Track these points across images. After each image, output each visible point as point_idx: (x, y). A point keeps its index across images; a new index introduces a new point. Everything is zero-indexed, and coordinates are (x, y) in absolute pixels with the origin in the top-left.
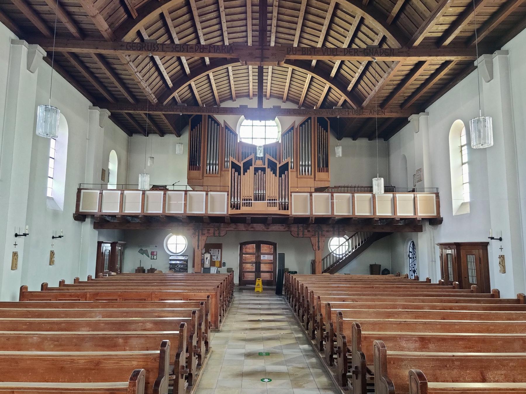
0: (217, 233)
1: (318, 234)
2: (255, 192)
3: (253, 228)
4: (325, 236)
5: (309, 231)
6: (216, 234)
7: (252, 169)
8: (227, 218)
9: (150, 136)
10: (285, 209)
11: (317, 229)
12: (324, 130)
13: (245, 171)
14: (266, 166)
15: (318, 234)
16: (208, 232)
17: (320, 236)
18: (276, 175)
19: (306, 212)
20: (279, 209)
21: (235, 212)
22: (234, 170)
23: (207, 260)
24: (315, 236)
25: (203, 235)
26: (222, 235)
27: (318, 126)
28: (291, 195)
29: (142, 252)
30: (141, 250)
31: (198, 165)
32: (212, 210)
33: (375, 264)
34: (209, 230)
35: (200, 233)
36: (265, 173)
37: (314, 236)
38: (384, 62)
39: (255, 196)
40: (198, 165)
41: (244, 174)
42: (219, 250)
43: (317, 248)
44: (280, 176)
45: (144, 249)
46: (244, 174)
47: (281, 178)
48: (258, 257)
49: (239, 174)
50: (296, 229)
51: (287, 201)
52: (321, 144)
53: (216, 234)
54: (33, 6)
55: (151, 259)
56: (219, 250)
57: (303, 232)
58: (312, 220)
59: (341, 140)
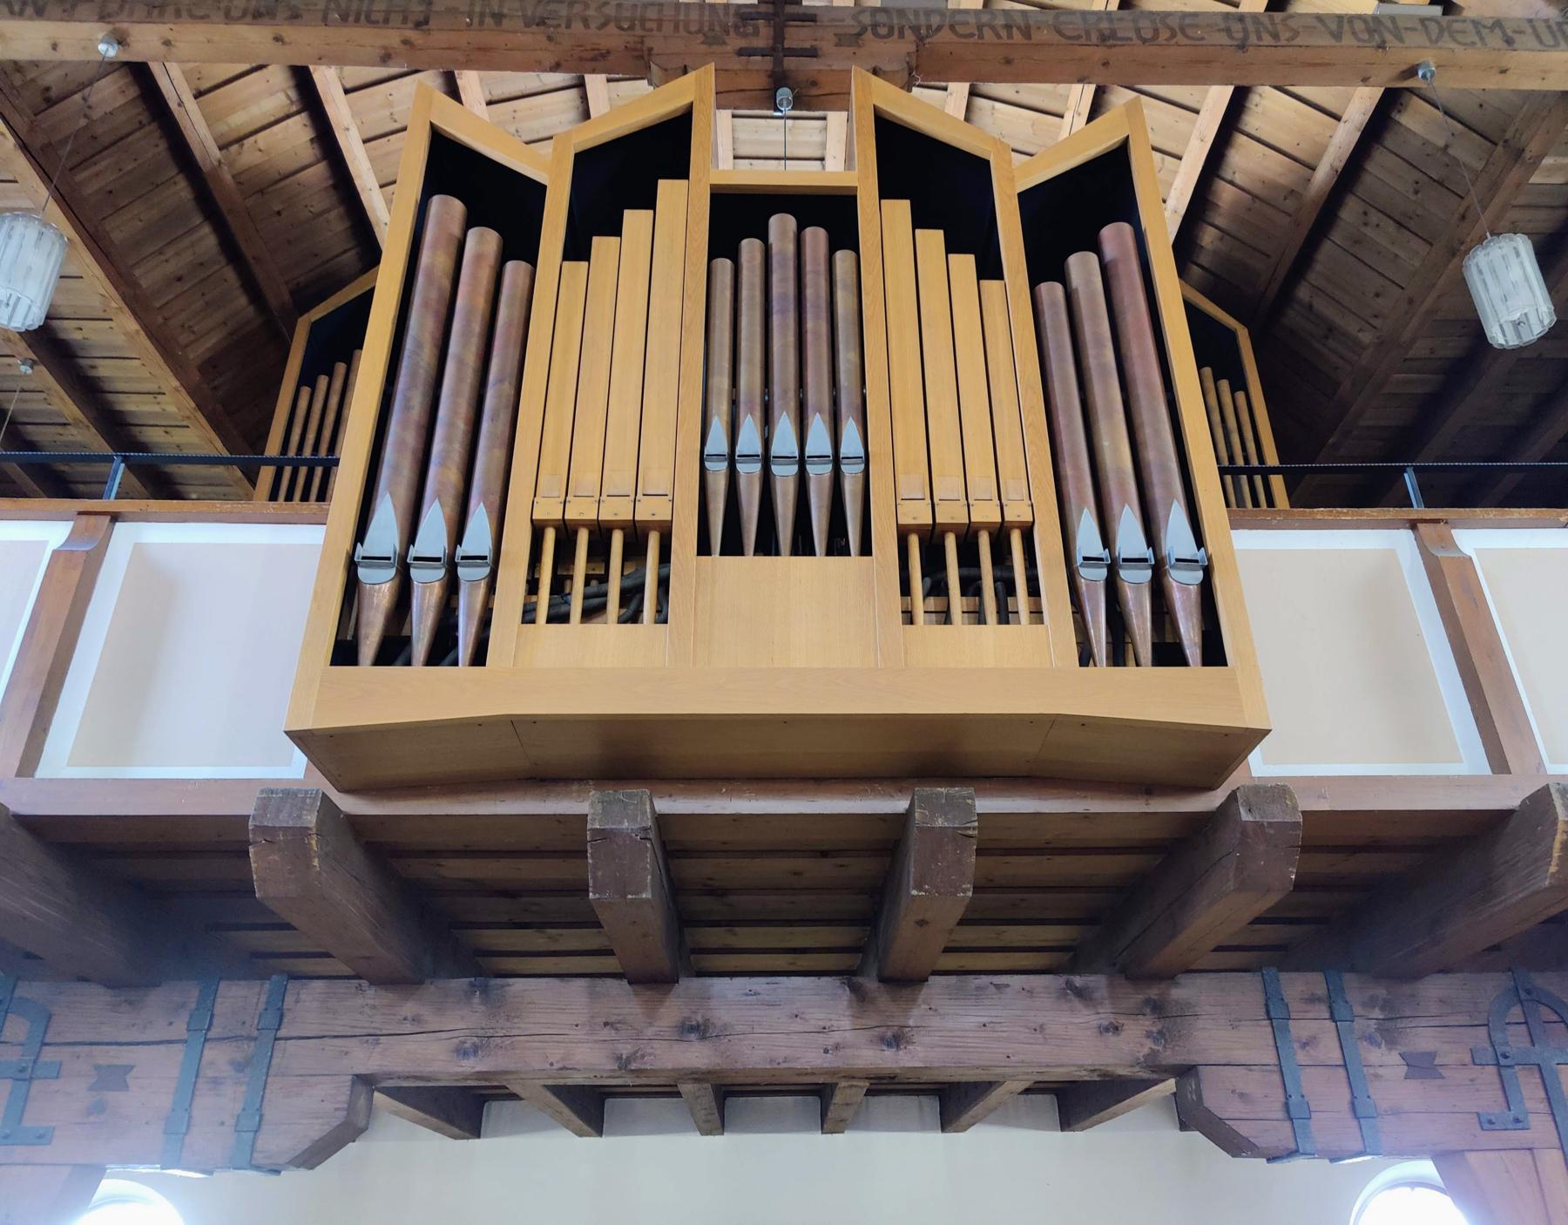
2: (718, 442)
3: (697, 1030)
8: (285, 820)
11: (1516, 1040)
14: (863, 179)
18: (990, 268)
39: (719, 485)
41: (577, 249)
46: (577, 249)
47: (1051, 291)
50: (1253, 1044)
54: (72, 486)
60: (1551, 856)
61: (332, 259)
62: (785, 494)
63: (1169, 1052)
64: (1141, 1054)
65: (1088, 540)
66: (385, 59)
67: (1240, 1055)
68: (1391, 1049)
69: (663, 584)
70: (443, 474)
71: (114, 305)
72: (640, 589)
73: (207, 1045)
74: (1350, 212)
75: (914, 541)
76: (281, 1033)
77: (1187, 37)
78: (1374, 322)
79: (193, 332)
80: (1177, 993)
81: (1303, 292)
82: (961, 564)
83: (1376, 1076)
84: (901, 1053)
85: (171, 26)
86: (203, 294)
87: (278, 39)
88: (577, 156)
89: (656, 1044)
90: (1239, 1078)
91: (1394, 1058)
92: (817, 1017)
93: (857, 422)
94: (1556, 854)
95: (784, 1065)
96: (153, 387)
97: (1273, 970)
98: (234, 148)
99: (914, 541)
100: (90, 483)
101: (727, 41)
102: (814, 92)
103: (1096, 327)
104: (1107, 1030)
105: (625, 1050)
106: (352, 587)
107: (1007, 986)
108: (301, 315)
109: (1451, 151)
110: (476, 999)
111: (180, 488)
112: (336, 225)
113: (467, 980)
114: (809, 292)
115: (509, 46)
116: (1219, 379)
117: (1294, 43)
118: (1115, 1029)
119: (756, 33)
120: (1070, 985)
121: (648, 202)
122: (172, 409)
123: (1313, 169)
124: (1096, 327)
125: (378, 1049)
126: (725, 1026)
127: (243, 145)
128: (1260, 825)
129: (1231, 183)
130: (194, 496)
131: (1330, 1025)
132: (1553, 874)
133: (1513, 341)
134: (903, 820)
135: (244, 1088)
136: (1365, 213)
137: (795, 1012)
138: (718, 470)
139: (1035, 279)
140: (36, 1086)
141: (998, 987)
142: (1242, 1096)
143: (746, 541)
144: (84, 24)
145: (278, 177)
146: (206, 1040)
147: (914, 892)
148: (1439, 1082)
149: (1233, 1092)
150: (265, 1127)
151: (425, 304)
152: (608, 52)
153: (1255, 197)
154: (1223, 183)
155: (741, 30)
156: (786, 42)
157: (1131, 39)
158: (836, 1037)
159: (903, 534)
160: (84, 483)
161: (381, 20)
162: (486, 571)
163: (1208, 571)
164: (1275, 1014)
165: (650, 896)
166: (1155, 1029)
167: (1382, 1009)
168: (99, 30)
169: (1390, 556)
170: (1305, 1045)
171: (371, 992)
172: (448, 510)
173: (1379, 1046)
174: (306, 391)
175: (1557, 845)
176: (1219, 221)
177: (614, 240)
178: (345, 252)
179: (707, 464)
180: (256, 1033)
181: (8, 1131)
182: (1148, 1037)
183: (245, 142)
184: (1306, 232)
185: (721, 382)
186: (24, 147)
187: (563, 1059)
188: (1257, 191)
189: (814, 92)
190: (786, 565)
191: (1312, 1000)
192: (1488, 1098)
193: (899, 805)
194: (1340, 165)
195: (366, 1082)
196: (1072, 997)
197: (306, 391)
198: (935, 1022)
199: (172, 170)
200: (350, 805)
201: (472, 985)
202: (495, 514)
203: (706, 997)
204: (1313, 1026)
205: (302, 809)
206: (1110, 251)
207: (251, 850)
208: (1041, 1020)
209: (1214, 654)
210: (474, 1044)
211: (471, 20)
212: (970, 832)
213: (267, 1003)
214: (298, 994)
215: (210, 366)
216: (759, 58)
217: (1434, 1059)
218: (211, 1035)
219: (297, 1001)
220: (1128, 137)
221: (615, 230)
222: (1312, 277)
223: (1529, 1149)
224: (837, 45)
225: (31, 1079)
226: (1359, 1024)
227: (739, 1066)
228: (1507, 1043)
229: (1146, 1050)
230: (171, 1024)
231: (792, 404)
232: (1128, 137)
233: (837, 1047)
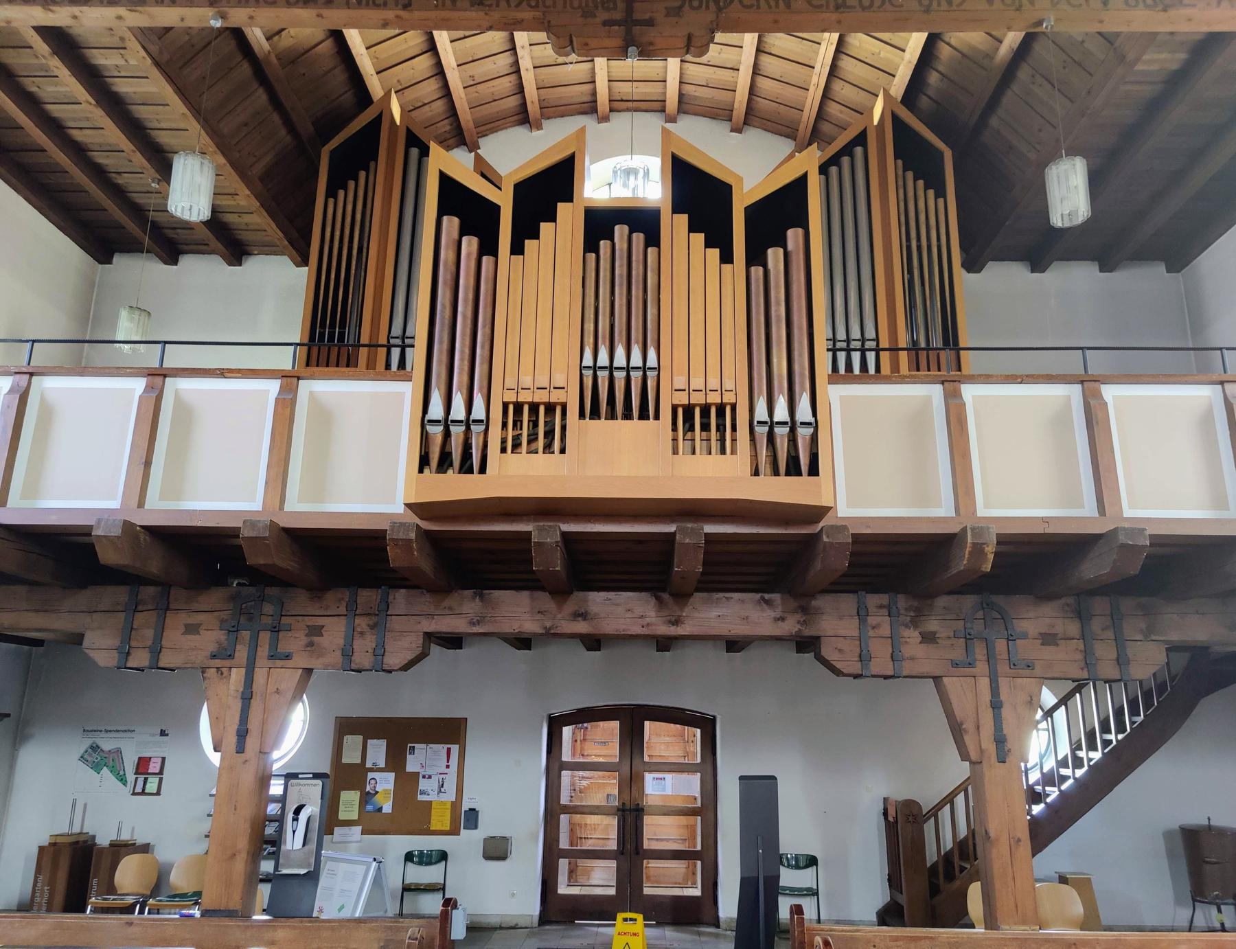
0: (363, 649)
1: (990, 657)
2: (588, 361)
3: (582, 615)
4: (1038, 670)
5: (929, 638)
6: (362, 656)
7: (569, 218)
8: (401, 536)
9: (186, 261)
10: (793, 469)
11: (978, 626)
12: (926, 188)
13: (525, 230)
15: (990, 657)
16: (311, 644)
17: (1003, 668)
18: (727, 258)
20: (756, 473)
22: (451, 224)
23: (295, 819)
24: (971, 665)
25: (279, 663)
26: (394, 659)
27: (900, 172)
29: (97, 759)
30: (95, 748)
33: (1210, 828)
34: (316, 631)
35: (263, 651)
36: (653, 239)
37: (963, 665)
38: (1099, 33)
39: (589, 382)
41: (517, 249)
42: (449, 750)
43: (989, 746)
44: (756, 256)
45: (107, 745)
46: (517, 249)
47: (757, 271)
48: (632, 782)
49: (489, 247)
50: (849, 627)
51: (804, 411)
52: (919, 248)
53: (362, 656)
55: (134, 794)
56: (449, 750)
57: (895, 641)
58: (978, 549)
59: (979, 271)
60: (964, 556)
61: (338, 98)
62: (620, 388)
63: (807, 630)
64: (794, 631)
65: (761, 413)
66: (385, 25)
67: (842, 632)
68: (915, 630)
69: (564, 428)
70: (459, 378)
71: (211, 150)
72: (553, 431)
73: (356, 617)
74: (1023, 74)
75: (680, 411)
76: (388, 613)
77: (893, 5)
78: (1037, 146)
79: (255, 156)
80: (814, 603)
81: (994, 121)
82: (701, 417)
83: (906, 642)
84: (679, 628)
85: (254, 9)
86: (260, 132)
87: (319, 16)
88: (514, 185)
89: (562, 622)
90: (841, 643)
91: (916, 634)
92: (638, 610)
93: (655, 348)
94: (967, 556)
95: (623, 633)
96: (232, 191)
97: (864, 593)
98: (276, 38)
99: (680, 411)
100: (190, 244)
101: (597, 14)
102: (651, 48)
103: (778, 294)
104: (778, 619)
105: (548, 624)
106: (425, 438)
107: (732, 598)
108: (324, 146)
109: (1086, 45)
110: (477, 599)
111: (248, 248)
112: (340, 76)
113: (472, 590)
114: (634, 273)
115: (461, 18)
116: (928, 189)
117: (961, 8)
118: (783, 619)
119: (615, 8)
120: (762, 598)
121: (552, 218)
122: (243, 203)
123: (1001, 42)
124: (778, 294)
125: (434, 621)
126: (596, 614)
127: (281, 36)
128: (831, 543)
129: (948, 44)
130: (256, 252)
131: (888, 618)
132: (965, 565)
133: (1067, 224)
134: (674, 534)
135: (375, 637)
136: (1033, 76)
137: (628, 608)
138: (588, 374)
139: (749, 263)
140: (281, 634)
141: (727, 598)
142: (840, 651)
143: (601, 411)
144: (202, 9)
145: (303, 51)
146: (355, 615)
147: (676, 569)
148: (936, 645)
149: (836, 648)
150: (386, 654)
151: (445, 283)
152: (522, 20)
153: (964, 55)
154: (943, 44)
155: (606, 5)
156: (634, 14)
157: (855, 7)
158: (648, 620)
159: (674, 409)
160: (187, 244)
161: (382, 3)
162: (484, 427)
163: (816, 428)
164: (862, 614)
165: (559, 569)
166: (802, 620)
167: (914, 611)
168: (210, 12)
169: (928, 399)
170: (873, 628)
171: (428, 595)
172: (465, 396)
173: (910, 629)
174: (331, 201)
175: (967, 552)
176: (940, 68)
177: (536, 241)
178: (346, 92)
179: (583, 372)
180: (377, 613)
181: (272, 654)
182: (798, 623)
183: (282, 33)
184: (643, 593)
185: (590, 326)
186: (157, 64)
187: (520, 628)
188: (965, 51)
189: (651, 48)
190: (620, 423)
191: (881, 607)
192: (958, 654)
193: (671, 528)
194: (1015, 46)
195: (430, 637)
196: (765, 605)
197: (331, 201)
198: (697, 615)
199: (255, 85)
200: (426, 525)
201: (475, 593)
202: (485, 399)
203: (586, 601)
204: (880, 622)
205: (408, 531)
206: (790, 246)
207: (388, 547)
208: (747, 614)
209: (814, 470)
210: (478, 620)
211: (437, 1)
212: (701, 545)
213: (381, 599)
214: (395, 595)
215: (265, 177)
216: (617, 27)
217: (935, 634)
218: (357, 613)
219: (394, 599)
220: (807, 172)
221: (536, 236)
222: (1000, 112)
223: (974, 677)
224: (666, 16)
225: (278, 631)
226: (902, 618)
227: (601, 633)
228: (972, 628)
229: (796, 629)
230: (338, 607)
231: (624, 339)
232: (807, 172)
233: (648, 624)
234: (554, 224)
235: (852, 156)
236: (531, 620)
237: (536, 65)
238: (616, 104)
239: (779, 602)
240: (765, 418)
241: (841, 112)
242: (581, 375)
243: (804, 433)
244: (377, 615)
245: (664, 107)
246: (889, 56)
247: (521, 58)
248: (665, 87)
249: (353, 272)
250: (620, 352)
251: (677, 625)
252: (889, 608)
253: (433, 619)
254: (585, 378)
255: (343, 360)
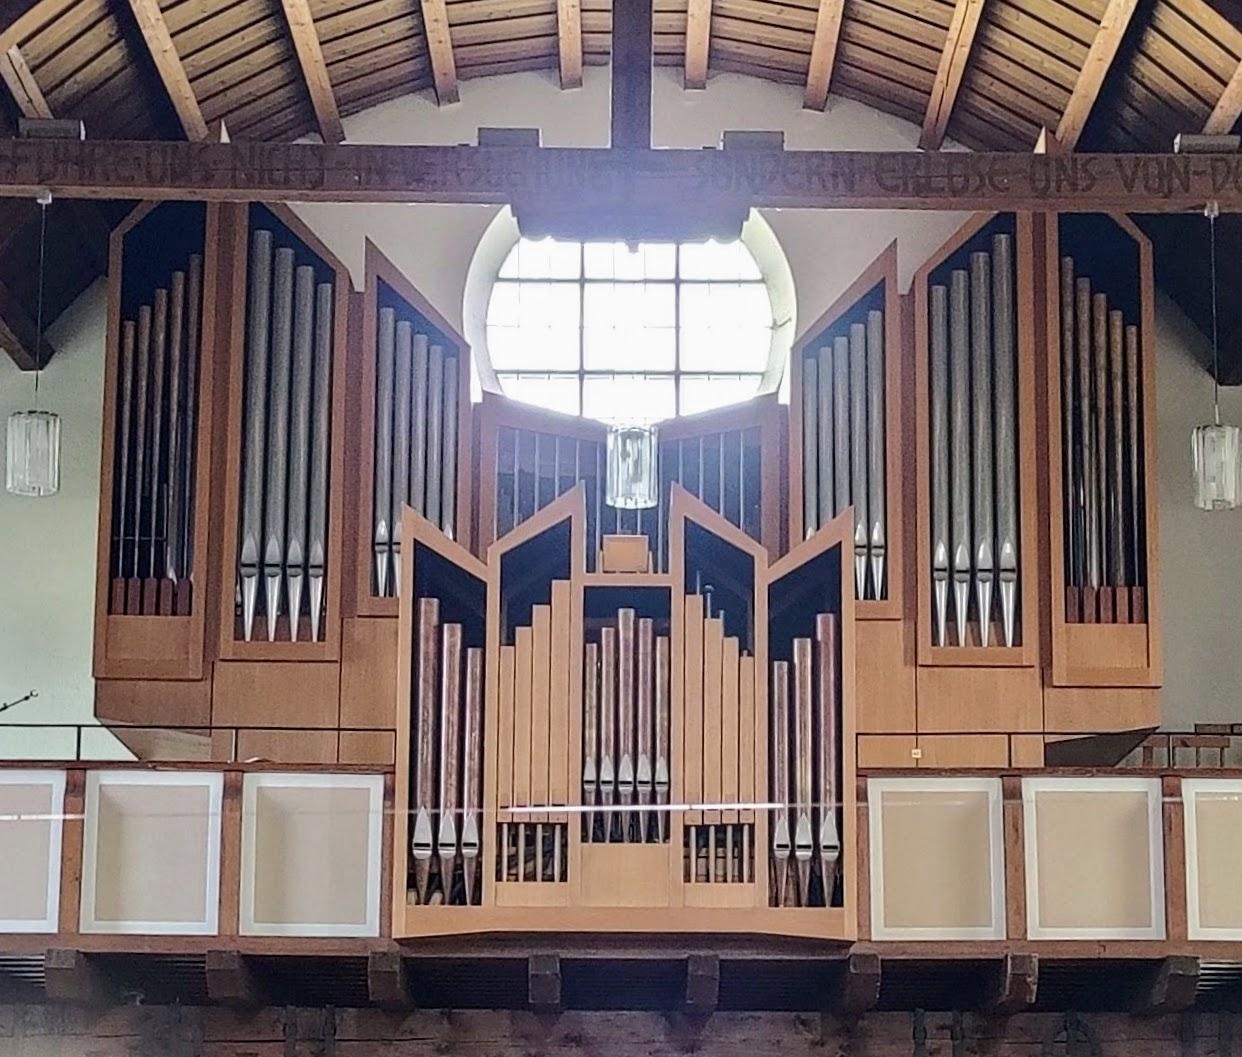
2: (590, 775)
7: (567, 595)
10: (815, 900)
12: (1110, 308)
13: (517, 616)
19: (972, 913)
20: (775, 902)
21: (443, 919)
22: (430, 607)
27: (1069, 280)
28: (862, 795)
31: (171, 574)
32: (275, 905)
36: (662, 630)
40: (171, 574)
44: (779, 651)
46: (510, 640)
49: (474, 637)
52: (1094, 408)
58: (1020, 980)
104: (817, 1044)
120: (798, 1017)
125: (392, 1048)
166: (845, 1044)
169: (1180, 751)
174: (130, 325)
180: (322, 1037)
185: (592, 734)
197: (130, 325)
234: (548, 607)
235: (990, 250)
236: (513, 1046)
237: (452, 23)
238: (589, 58)
239: (818, 1021)
240: (786, 840)
241: (993, 109)
242: (583, 791)
243: (828, 856)
244: (323, 1040)
245: (684, 60)
246: (1055, 68)
247: (431, 32)
248: (685, 40)
249: (188, 483)
250: (626, 761)
251: (692, 1052)
252: (951, 1029)
253: (391, 1044)
254: (587, 795)
255: (166, 603)
